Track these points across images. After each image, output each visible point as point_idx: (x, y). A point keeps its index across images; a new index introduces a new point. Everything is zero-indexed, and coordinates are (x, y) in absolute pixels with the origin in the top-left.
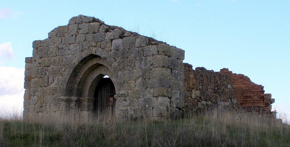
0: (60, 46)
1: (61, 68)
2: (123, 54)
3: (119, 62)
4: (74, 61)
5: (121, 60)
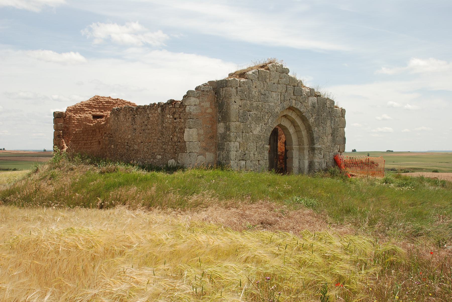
1: (265, 116)
3: (315, 118)
4: (276, 110)
5: (317, 117)
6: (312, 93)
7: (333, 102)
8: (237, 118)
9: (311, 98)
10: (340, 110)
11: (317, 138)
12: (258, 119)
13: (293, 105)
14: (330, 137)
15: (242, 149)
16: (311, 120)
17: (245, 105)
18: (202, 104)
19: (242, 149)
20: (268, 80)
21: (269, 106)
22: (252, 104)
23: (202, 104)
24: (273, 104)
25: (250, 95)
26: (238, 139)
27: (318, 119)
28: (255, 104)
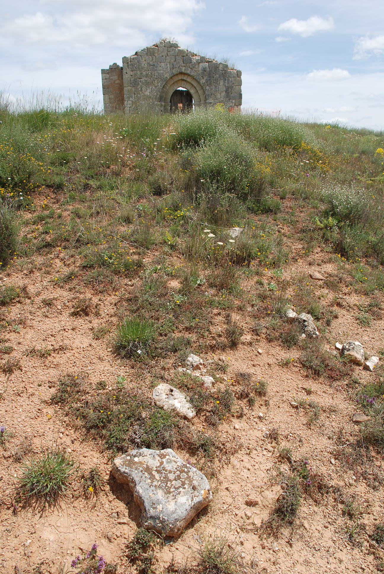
0: (151, 63)
2: (209, 74)
3: (206, 80)
4: (165, 76)
6: (203, 60)
7: (227, 66)
8: (129, 84)
9: (201, 64)
10: (235, 71)
11: (209, 95)
12: (147, 84)
13: (183, 71)
14: (224, 94)
15: (134, 105)
16: (203, 81)
17: (136, 75)
18: (111, 78)
19: (134, 105)
20: (156, 55)
21: (159, 73)
22: (142, 74)
23: (111, 78)
24: (162, 72)
25: (140, 67)
26: (131, 99)
27: (210, 80)
28: (144, 73)
